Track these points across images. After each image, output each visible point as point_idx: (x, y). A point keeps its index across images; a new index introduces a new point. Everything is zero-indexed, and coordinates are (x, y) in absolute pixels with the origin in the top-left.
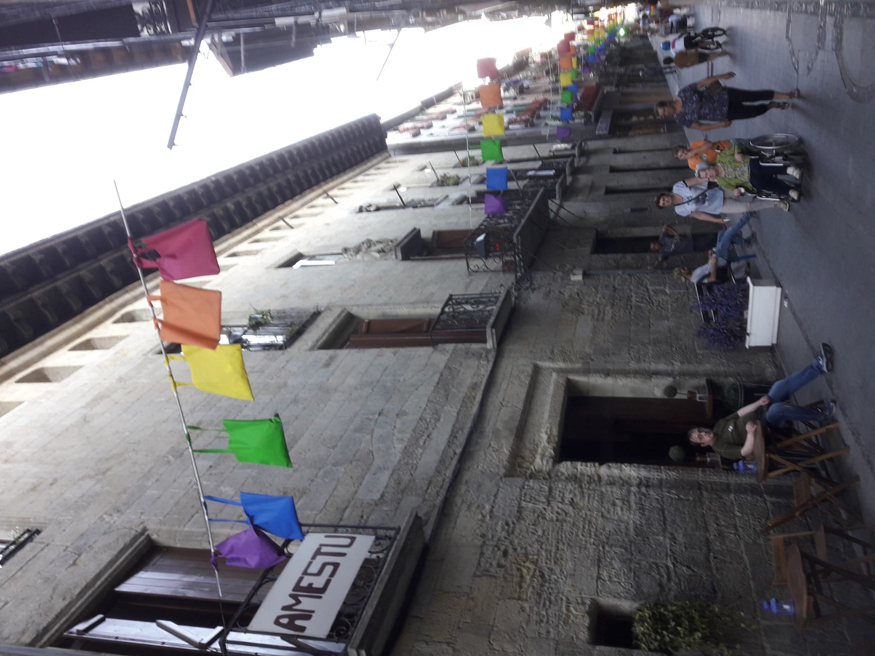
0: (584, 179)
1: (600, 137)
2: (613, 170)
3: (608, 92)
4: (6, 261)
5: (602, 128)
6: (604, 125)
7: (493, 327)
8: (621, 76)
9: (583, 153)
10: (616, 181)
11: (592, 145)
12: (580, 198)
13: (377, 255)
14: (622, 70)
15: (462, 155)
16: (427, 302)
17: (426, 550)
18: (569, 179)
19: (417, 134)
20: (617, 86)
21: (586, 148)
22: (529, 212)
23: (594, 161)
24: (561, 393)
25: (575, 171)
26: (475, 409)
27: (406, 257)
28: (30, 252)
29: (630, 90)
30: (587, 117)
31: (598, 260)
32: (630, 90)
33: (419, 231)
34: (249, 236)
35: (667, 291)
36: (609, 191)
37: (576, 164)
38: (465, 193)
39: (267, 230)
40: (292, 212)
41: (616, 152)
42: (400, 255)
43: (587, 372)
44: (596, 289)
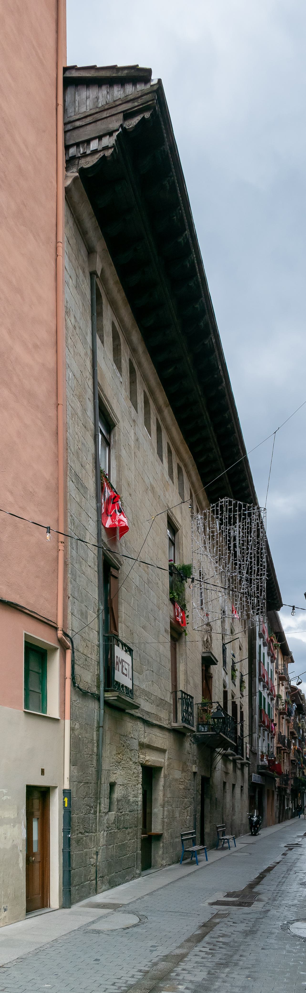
0: (231, 766)
1: (250, 777)
2: (234, 785)
3: (275, 781)
4: (231, 412)
5: (256, 778)
6: (257, 779)
7: (184, 727)
8: (285, 790)
9: (243, 765)
10: (229, 787)
11: (246, 770)
12: (223, 766)
13: (205, 639)
14: (288, 791)
15: (246, 679)
16: (187, 682)
17: (122, 711)
18: (231, 758)
19: (261, 636)
20: (279, 787)
21: (245, 767)
22: (228, 739)
23: (239, 772)
24: (158, 765)
25: (234, 761)
26: (155, 722)
27: (203, 658)
28: (237, 434)
29: (276, 797)
30: (263, 767)
31: (199, 778)
32: (276, 797)
33: (216, 664)
34: (121, 321)
35: (188, 817)
36: (225, 783)
37: (237, 761)
38: (228, 687)
39: (178, 461)
40: (186, 466)
41: (242, 787)
42: (205, 655)
43: (165, 777)
44: (190, 780)
